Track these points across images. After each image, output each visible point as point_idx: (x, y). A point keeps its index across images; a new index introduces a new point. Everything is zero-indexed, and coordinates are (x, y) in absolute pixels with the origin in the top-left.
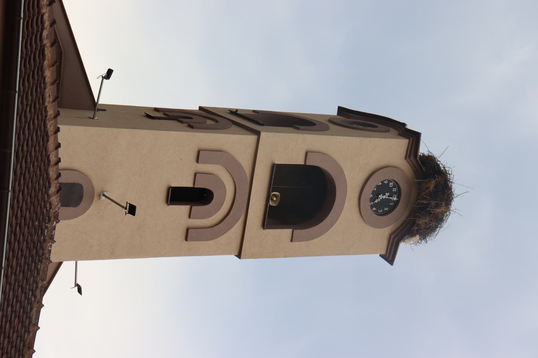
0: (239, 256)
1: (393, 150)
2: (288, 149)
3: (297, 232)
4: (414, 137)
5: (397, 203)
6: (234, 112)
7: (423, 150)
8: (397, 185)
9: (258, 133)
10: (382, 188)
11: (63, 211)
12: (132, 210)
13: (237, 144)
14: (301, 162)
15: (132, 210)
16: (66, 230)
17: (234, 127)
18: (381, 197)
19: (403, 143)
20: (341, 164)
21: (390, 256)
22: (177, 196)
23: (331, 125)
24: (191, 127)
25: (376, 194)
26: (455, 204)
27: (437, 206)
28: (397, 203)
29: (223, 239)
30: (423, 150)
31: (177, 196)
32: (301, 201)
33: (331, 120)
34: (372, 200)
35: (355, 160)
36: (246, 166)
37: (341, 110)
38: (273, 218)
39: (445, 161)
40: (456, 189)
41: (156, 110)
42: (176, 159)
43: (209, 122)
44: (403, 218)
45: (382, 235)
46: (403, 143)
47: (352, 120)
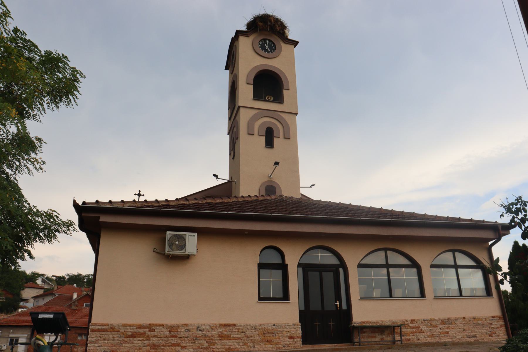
0: (296, 114)
1: (245, 43)
2: (246, 92)
3: (285, 87)
4: (238, 33)
5: (270, 41)
6: (230, 118)
7: (244, 29)
8: (261, 41)
9: (239, 107)
10: (263, 48)
11: (278, 193)
12: (277, 163)
13: (244, 116)
14: (252, 86)
15: (277, 163)
16: (286, 192)
17: (237, 118)
18: (267, 48)
19: (241, 38)
20: (252, 67)
21: (295, 43)
22: (269, 144)
23: (234, 73)
24: (237, 138)
25: (266, 51)
26: (269, 13)
27: (270, 21)
28: (270, 41)
29: (289, 122)
30: (244, 29)
31: (269, 144)
32: (270, 85)
33: (231, 73)
34: (268, 52)
35: (250, 61)
36: (255, 112)
37: (227, 68)
38: (278, 98)
39: (249, 19)
40: (262, 12)
41: (230, 154)
42: (253, 144)
43: (235, 130)
44: (277, 38)
45: (285, 47)
46: (241, 38)
47: (231, 63)
